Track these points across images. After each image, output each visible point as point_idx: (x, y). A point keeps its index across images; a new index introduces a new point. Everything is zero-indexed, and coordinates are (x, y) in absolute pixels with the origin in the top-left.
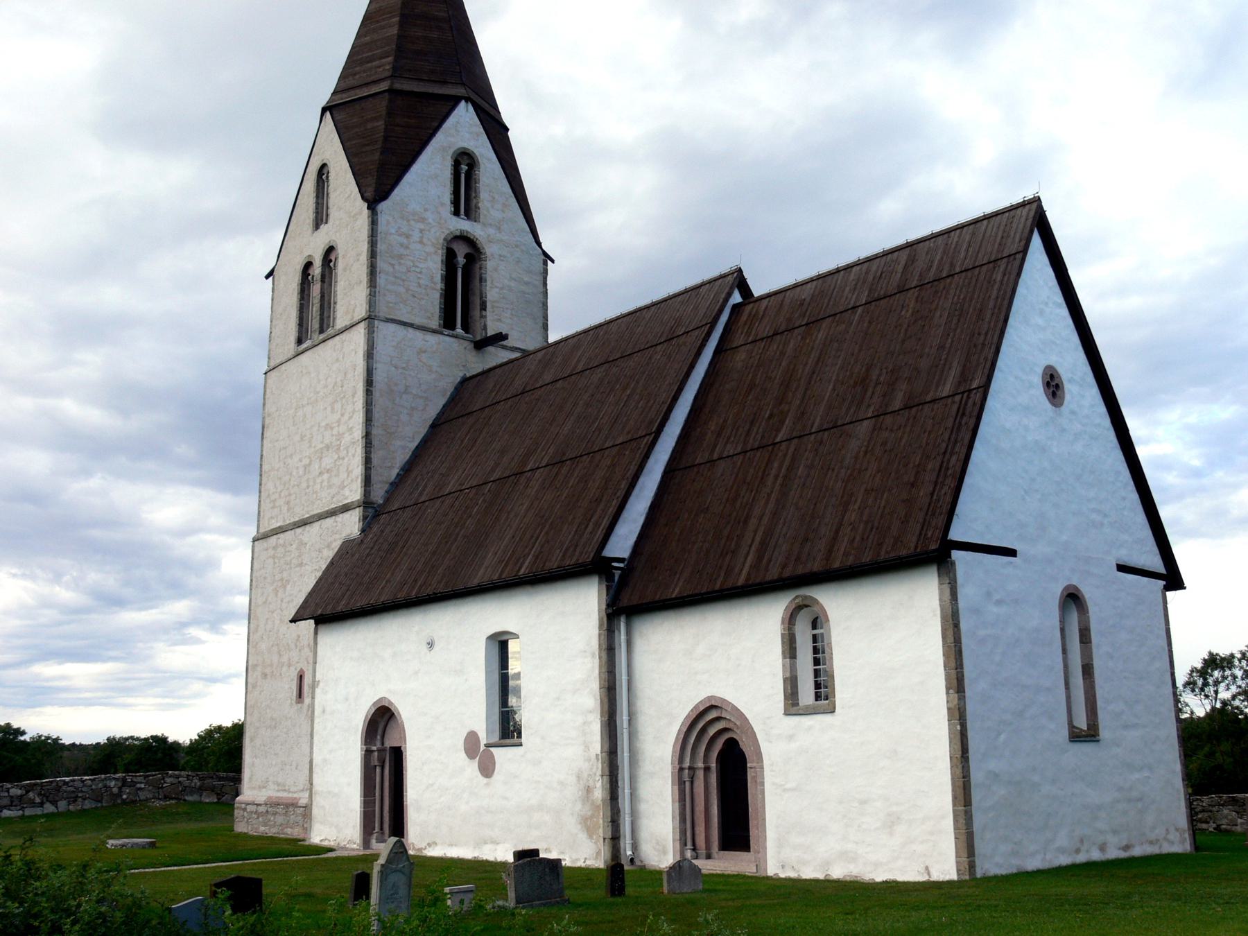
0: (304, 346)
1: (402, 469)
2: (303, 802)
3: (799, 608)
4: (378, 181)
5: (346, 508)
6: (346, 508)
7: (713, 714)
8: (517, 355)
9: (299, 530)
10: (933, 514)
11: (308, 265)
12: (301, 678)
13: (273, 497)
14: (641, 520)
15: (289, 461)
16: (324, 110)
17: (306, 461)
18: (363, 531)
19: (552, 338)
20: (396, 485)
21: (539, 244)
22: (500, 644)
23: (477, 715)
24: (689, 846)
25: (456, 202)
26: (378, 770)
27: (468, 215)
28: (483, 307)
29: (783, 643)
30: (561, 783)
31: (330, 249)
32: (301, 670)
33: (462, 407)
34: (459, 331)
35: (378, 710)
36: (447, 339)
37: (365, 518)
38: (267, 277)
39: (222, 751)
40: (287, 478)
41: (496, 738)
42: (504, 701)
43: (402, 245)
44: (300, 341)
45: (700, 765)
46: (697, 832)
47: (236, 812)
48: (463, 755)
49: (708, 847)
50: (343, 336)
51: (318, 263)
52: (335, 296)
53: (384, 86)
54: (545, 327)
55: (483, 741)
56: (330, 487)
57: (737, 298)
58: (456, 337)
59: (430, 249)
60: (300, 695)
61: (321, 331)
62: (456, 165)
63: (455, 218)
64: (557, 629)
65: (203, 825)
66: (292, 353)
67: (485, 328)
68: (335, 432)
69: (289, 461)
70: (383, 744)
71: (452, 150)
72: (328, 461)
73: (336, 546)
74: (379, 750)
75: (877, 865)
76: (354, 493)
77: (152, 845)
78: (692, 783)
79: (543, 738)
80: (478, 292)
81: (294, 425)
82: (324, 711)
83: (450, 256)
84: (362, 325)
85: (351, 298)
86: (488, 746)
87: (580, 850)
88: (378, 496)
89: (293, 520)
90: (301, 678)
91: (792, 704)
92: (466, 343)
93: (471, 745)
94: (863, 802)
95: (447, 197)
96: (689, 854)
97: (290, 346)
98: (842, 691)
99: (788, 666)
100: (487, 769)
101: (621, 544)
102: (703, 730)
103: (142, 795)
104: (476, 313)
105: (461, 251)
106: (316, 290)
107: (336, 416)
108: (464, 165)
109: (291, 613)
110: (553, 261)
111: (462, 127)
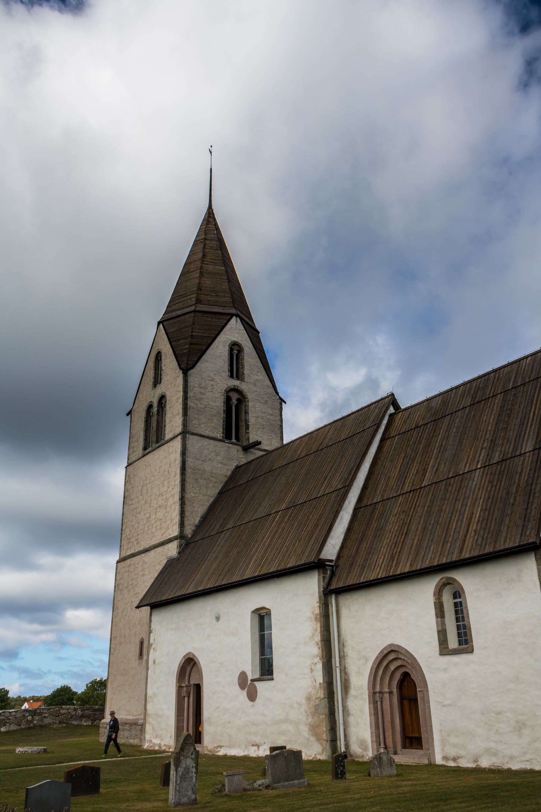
0: (147, 451)
1: (202, 518)
2: (141, 722)
3: (445, 585)
4: (188, 362)
5: (170, 541)
6: (170, 541)
7: (392, 656)
9: (143, 555)
10: (529, 521)
11: (150, 406)
12: (142, 643)
13: (129, 537)
14: (342, 537)
15: (138, 515)
16: (159, 323)
17: (148, 515)
18: (179, 553)
19: (285, 442)
20: (199, 527)
21: (277, 394)
22: (262, 617)
23: (249, 665)
24: (382, 745)
25: (231, 371)
26: (186, 699)
27: (238, 378)
28: (247, 427)
29: (435, 608)
30: (298, 703)
31: (162, 398)
32: (142, 639)
33: (235, 488)
34: (234, 440)
35: (186, 660)
36: (227, 444)
37: (181, 546)
38: (128, 415)
39: (97, 691)
40: (137, 525)
41: (257, 676)
42: (262, 652)
43: (201, 393)
44: (145, 448)
45: (386, 690)
46: (387, 736)
47: (101, 730)
48: (238, 687)
49: (395, 747)
50: (169, 444)
51: (155, 405)
52: (165, 422)
53: (192, 308)
54: (283, 440)
55: (250, 677)
56: (161, 529)
57: (392, 410)
58: (233, 443)
59: (217, 395)
60: (141, 654)
61: (157, 442)
62: (231, 350)
63: (231, 380)
64: (295, 603)
65: (81, 739)
66: (141, 455)
67: (248, 439)
68: (164, 498)
69: (138, 515)
70: (189, 682)
71: (230, 342)
72: (160, 515)
73: (165, 562)
74: (186, 686)
75: (512, 758)
76: (175, 531)
78: (382, 702)
79: (286, 674)
80: (243, 419)
81: (141, 495)
82: (154, 662)
83: (228, 400)
84: (179, 438)
85: (173, 423)
86: (253, 680)
87: (314, 750)
88: (189, 531)
89: (139, 549)
90: (142, 643)
91: (444, 649)
92: (238, 448)
93: (243, 681)
94: (499, 713)
95: (226, 367)
96: (382, 750)
97: (139, 451)
98: (477, 640)
99: (440, 623)
100: (252, 696)
101: (331, 550)
102: (387, 666)
103: (47, 721)
104: (243, 430)
105: (234, 397)
106: (154, 419)
107: (165, 488)
108: (235, 351)
109: (136, 603)
110: (285, 403)
111: (234, 332)
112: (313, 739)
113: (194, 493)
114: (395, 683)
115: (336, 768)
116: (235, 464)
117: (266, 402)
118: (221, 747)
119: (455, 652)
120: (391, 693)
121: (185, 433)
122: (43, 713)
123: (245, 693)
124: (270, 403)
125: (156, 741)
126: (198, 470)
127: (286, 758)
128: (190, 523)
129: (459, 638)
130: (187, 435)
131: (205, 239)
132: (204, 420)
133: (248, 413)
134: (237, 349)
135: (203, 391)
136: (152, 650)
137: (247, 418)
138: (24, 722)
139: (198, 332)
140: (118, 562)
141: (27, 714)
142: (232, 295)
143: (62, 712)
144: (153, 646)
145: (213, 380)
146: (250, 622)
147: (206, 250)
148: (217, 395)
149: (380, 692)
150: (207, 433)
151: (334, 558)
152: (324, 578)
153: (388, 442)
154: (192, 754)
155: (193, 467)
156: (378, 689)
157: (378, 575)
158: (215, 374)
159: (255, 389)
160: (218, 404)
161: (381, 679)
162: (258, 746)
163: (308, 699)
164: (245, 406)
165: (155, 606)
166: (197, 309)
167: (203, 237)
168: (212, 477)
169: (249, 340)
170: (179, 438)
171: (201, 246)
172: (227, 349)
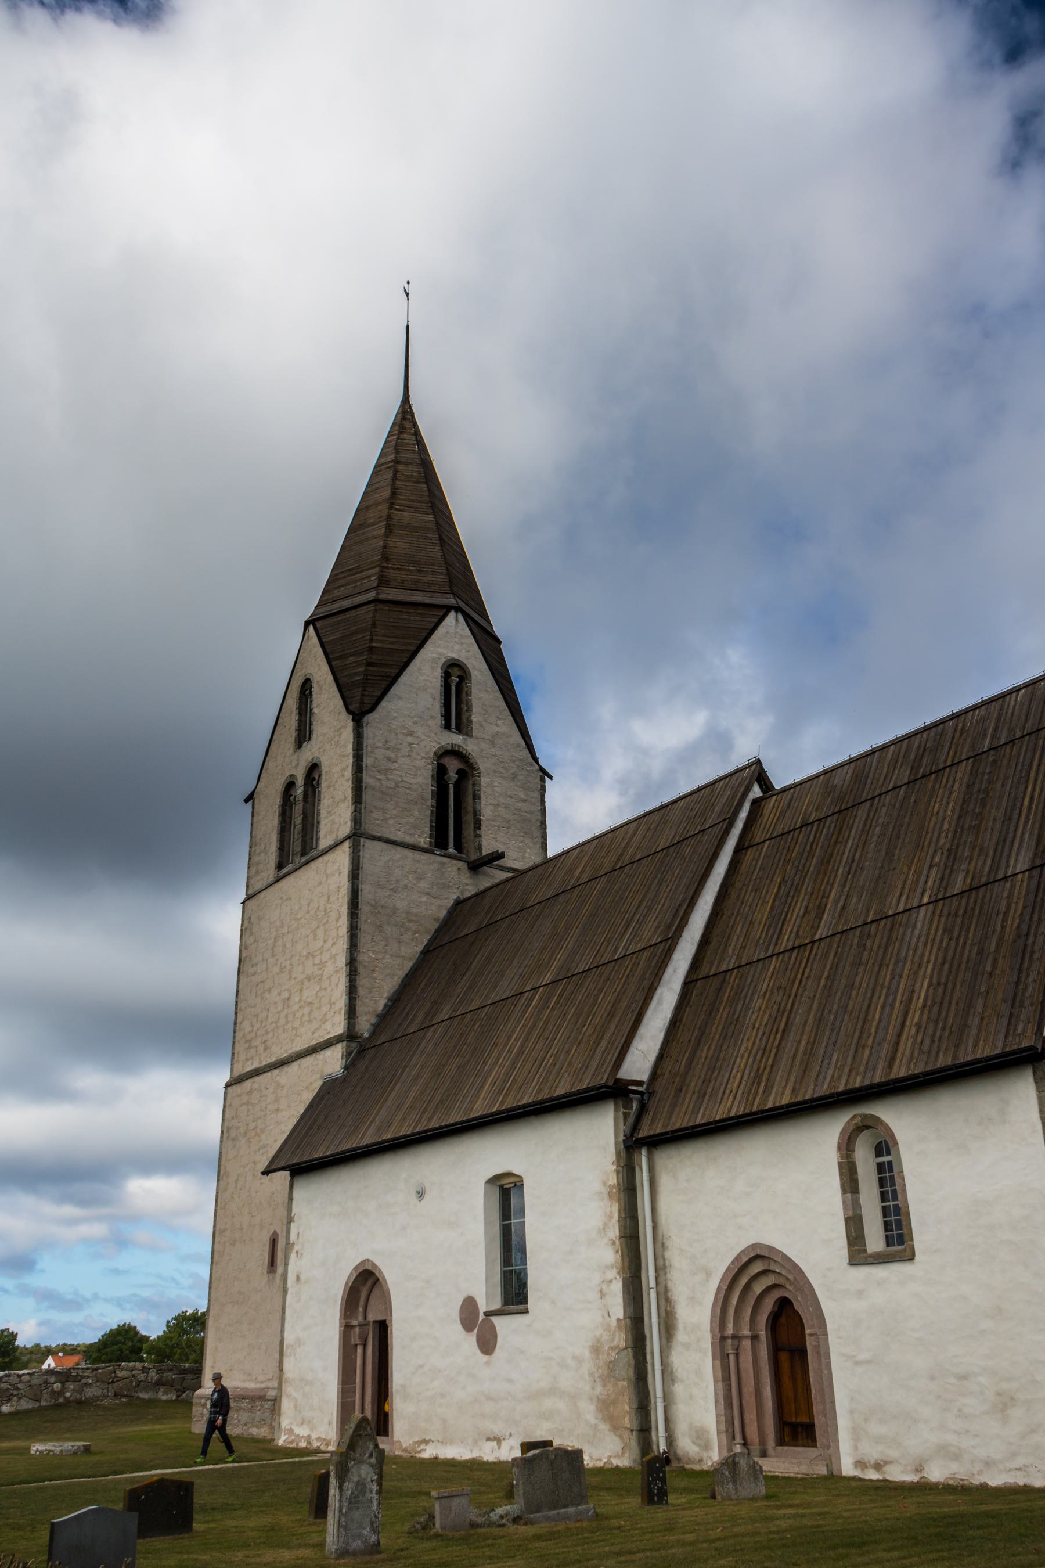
0: (284, 871)
1: (389, 999)
2: (272, 1393)
3: (860, 1129)
5: (328, 1044)
6: (328, 1044)
7: (757, 1267)
8: (510, 875)
9: (276, 1072)
10: (1021, 1006)
11: (290, 785)
12: (274, 1242)
13: (248, 1037)
14: (661, 1036)
15: (267, 995)
16: (307, 624)
17: (285, 995)
18: (346, 1068)
19: (551, 854)
20: (384, 1018)
21: (536, 760)
22: (506, 1192)
23: (481, 1284)
24: (738, 1439)
25: (447, 716)
26: (359, 1350)
27: (459, 730)
28: (478, 824)
29: (841, 1174)
30: (575, 1358)
31: (314, 768)
32: (275, 1233)
33: (454, 943)
34: (451, 850)
35: (359, 1275)
36: (439, 858)
37: (349, 1054)
38: (246, 801)
39: (188, 1334)
40: (264, 1014)
41: (497, 1305)
42: (507, 1259)
43: (389, 759)
44: (280, 866)
45: (746, 1332)
46: (747, 1421)
47: (194, 1409)
48: (459, 1327)
49: (763, 1442)
50: (326, 858)
51: (300, 781)
52: (319, 815)
53: (372, 595)
54: (546, 850)
55: (483, 1308)
56: (310, 1021)
57: (756, 792)
58: (449, 856)
59: (420, 763)
60: (272, 1263)
61: (303, 854)
62: (447, 676)
63: (446, 733)
64: (569, 1165)
65: (157, 1427)
66: (272, 879)
67: (480, 848)
68: (317, 961)
69: (267, 995)
70: (365, 1318)
71: (444, 660)
72: (309, 994)
73: (318, 1084)
74: (360, 1325)
75: (988, 1463)
76: (337, 1026)
77: (87, 1450)
78: (737, 1355)
79: (553, 1302)
80: (470, 808)
81: (273, 956)
82: (298, 1278)
83: (441, 772)
84: (347, 845)
85: (335, 816)
86: (488, 1314)
87: (606, 1449)
88: (365, 1025)
89: (269, 1061)
90: (274, 1242)
91: (858, 1254)
92: (461, 864)
93: (469, 1314)
94: (964, 1377)
95: (437, 708)
96: (738, 1449)
97: (269, 871)
98: (921, 1236)
99: (849, 1203)
100: (487, 1344)
101: (639, 1062)
102: (748, 1287)
103: (90, 1392)
104: (469, 831)
105: (453, 766)
106: (298, 810)
107: (319, 943)
108: (454, 677)
109: (263, 1165)
110: (551, 778)
111: (451, 640)
112: (604, 1427)
113: (374, 952)
114: (763, 1319)
115: (649, 1483)
116: (455, 897)
117: (514, 777)
118: (426, 1442)
119: (879, 1259)
120: (755, 1338)
121: (357, 836)
122: (83, 1377)
123: (472, 1338)
124: (521, 777)
125: (302, 1431)
126: (382, 907)
127: (552, 1463)
128: (366, 1009)
129: (886, 1231)
130: (362, 840)
131: (397, 462)
132: (394, 812)
133: (479, 798)
134: (459, 673)
135: (393, 755)
136: (293, 1256)
137: (477, 806)
138: (46, 1395)
139: (382, 642)
140: (228, 1085)
141: (52, 1379)
142: (447, 569)
143: (120, 1374)
144: (296, 1248)
145: (411, 734)
146: (482, 1201)
147: (398, 482)
148: (420, 763)
149: (735, 1337)
150: (399, 836)
151: (645, 1077)
152: (626, 1116)
153: (750, 854)
154: (371, 1456)
155: (373, 903)
156: (730, 1331)
157: (730, 1111)
158: (415, 723)
159: (493, 751)
160: (420, 780)
161: (736, 1312)
162: (499, 1440)
163: (596, 1349)
164: (474, 785)
165: (300, 1170)
166: (381, 597)
167: (392, 457)
168: (410, 921)
169: (481, 656)
170: (347, 845)
171: (389, 475)
172: (439, 673)
